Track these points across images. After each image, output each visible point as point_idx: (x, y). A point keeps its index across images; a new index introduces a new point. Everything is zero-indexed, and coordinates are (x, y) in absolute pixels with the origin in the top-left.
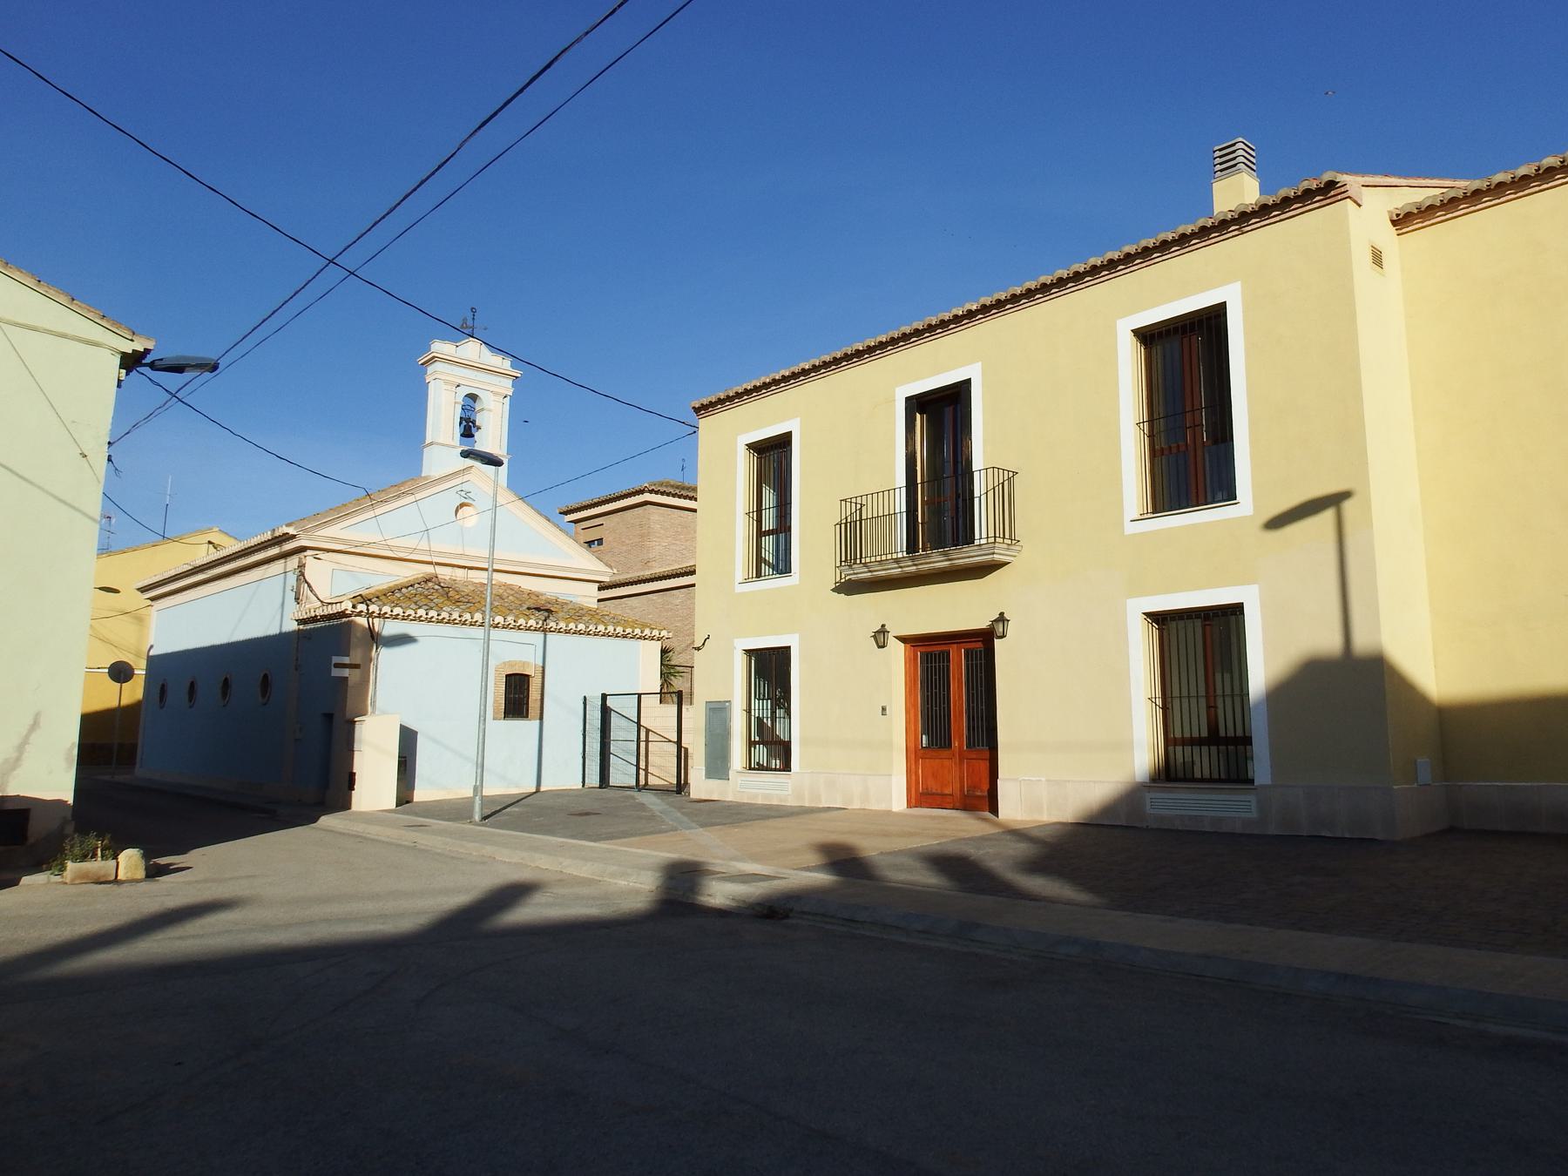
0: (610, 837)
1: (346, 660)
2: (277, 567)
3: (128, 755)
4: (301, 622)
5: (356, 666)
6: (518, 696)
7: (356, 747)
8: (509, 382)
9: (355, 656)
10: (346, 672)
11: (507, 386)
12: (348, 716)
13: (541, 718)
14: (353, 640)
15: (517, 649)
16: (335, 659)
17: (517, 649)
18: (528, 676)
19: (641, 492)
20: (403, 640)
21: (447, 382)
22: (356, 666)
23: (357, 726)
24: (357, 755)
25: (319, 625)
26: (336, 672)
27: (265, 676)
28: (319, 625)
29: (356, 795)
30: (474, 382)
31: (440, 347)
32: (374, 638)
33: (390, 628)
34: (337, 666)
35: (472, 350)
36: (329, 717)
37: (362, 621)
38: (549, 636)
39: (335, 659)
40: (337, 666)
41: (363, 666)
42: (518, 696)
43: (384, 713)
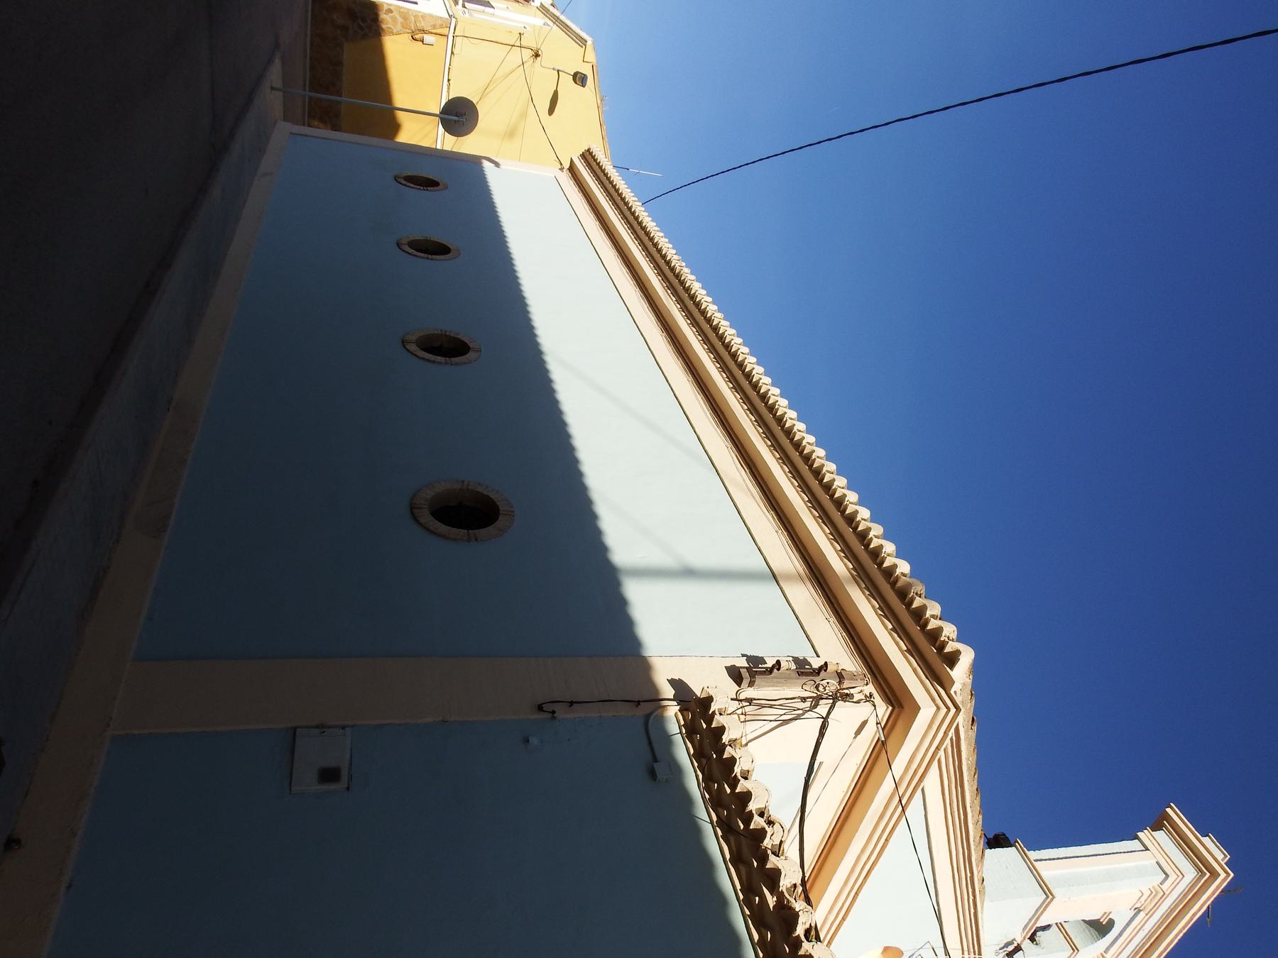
4: (697, 708)
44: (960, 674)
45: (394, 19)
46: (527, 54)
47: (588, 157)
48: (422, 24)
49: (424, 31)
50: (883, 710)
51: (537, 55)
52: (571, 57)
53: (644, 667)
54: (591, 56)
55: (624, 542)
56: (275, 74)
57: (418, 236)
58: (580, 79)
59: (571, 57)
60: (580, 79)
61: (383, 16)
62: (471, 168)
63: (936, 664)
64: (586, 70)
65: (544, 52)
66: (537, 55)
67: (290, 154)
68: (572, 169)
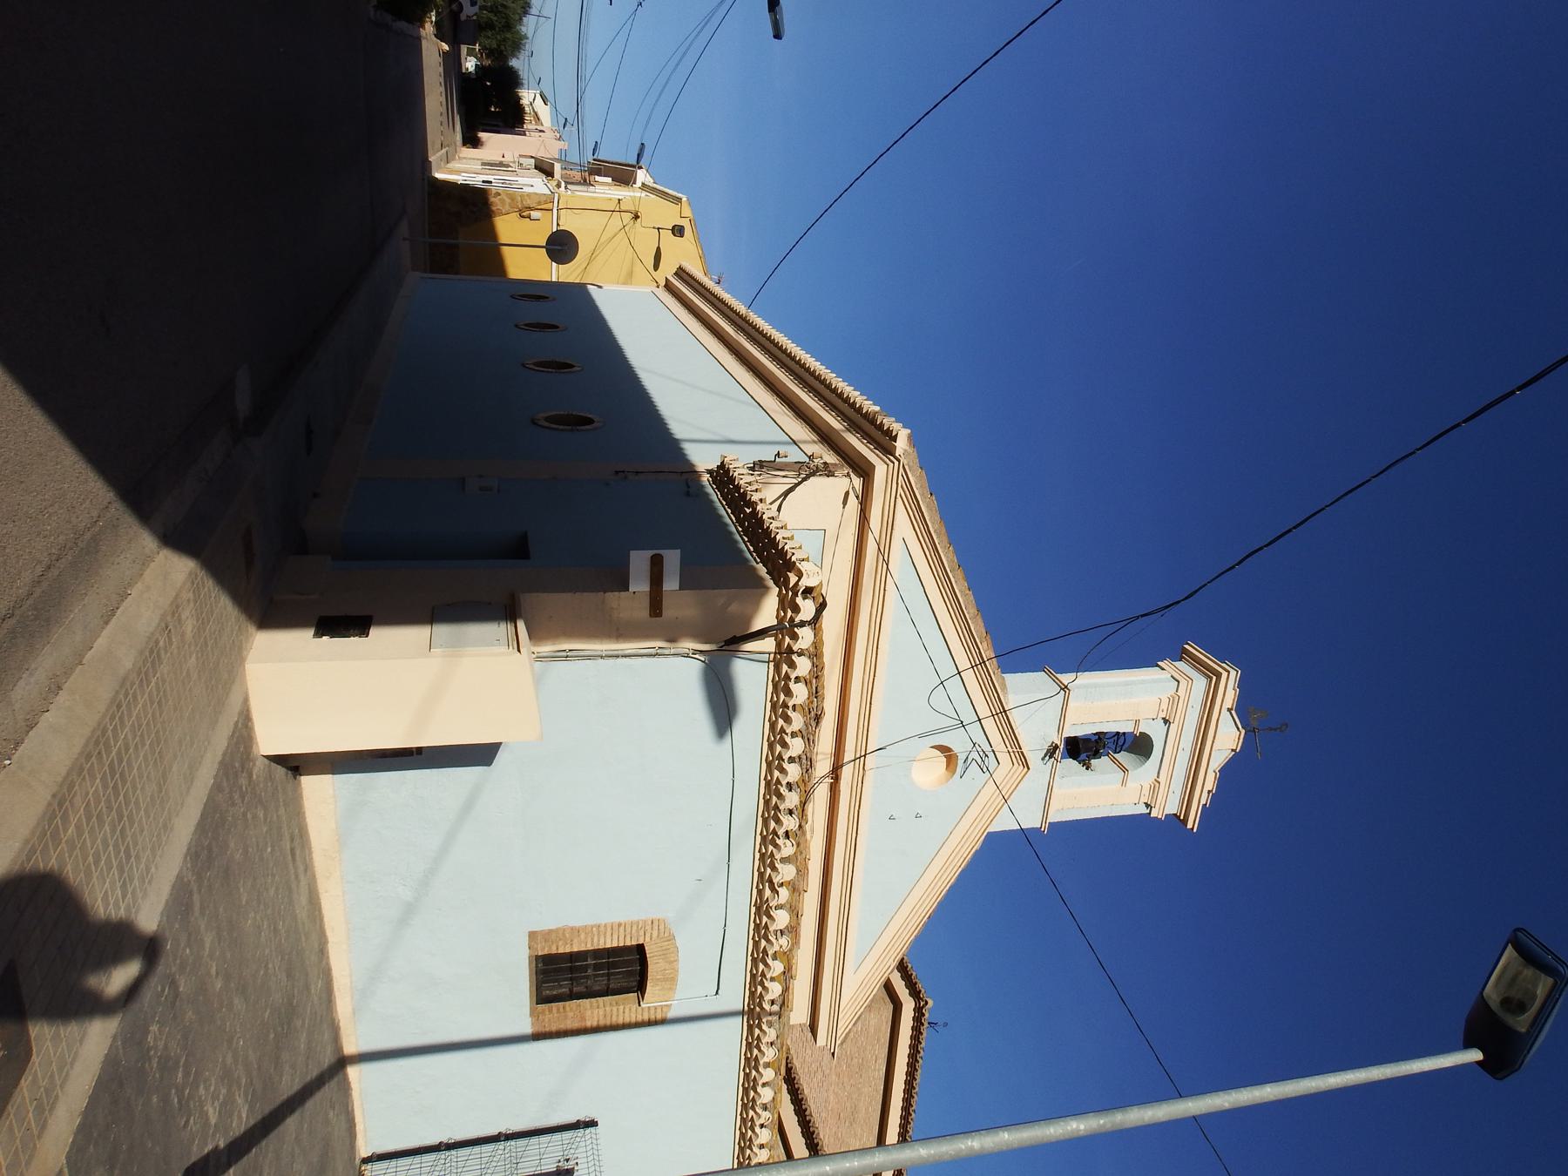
0: (327, 974)
1: (671, 584)
2: (799, 430)
3: (443, 260)
4: (722, 476)
5: (656, 607)
6: (590, 978)
7: (443, 631)
8: (1172, 808)
9: (680, 603)
10: (640, 585)
11: (1168, 805)
12: (528, 600)
13: (537, 1037)
14: (720, 597)
15: (701, 968)
16: (672, 559)
17: (701, 968)
18: (640, 987)
19: (915, 993)
20: (723, 709)
21: (1174, 700)
22: (656, 607)
23: (499, 630)
24: (416, 635)
25: (724, 512)
26: (639, 561)
27: (590, 421)
28: (724, 512)
29: (300, 641)
30: (1173, 752)
31: (1230, 680)
32: (733, 641)
33: (751, 677)
34: (657, 564)
35: (1227, 738)
36: (519, 550)
37: (767, 613)
38: (736, 1026)
39: (672, 559)
40: (657, 564)
41: (656, 622)
42: (590, 978)
43: (538, 680)
44: (901, 444)
45: (503, 201)
46: (627, 217)
47: (681, 273)
48: (528, 202)
49: (530, 209)
50: (857, 482)
51: (636, 217)
52: (669, 215)
53: (672, 447)
54: (687, 212)
55: (678, 429)
56: (403, 229)
57: (797, 1063)
58: (678, 231)
59: (669, 215)
60: (678, 231)
61: (492, 199)
62: (578, 294)
63: (887, 449)
64: (685, 223)
65: (642, 212)
66: (636, 217)
67: (420, 297)
68: (668, 287)
